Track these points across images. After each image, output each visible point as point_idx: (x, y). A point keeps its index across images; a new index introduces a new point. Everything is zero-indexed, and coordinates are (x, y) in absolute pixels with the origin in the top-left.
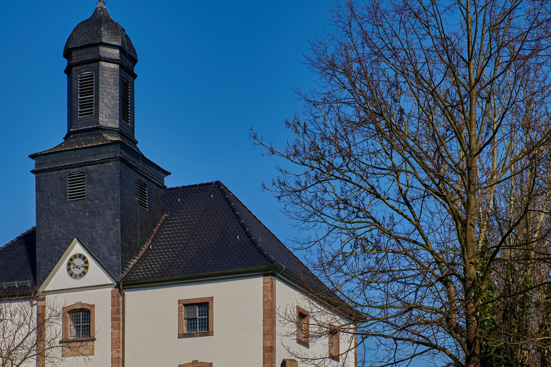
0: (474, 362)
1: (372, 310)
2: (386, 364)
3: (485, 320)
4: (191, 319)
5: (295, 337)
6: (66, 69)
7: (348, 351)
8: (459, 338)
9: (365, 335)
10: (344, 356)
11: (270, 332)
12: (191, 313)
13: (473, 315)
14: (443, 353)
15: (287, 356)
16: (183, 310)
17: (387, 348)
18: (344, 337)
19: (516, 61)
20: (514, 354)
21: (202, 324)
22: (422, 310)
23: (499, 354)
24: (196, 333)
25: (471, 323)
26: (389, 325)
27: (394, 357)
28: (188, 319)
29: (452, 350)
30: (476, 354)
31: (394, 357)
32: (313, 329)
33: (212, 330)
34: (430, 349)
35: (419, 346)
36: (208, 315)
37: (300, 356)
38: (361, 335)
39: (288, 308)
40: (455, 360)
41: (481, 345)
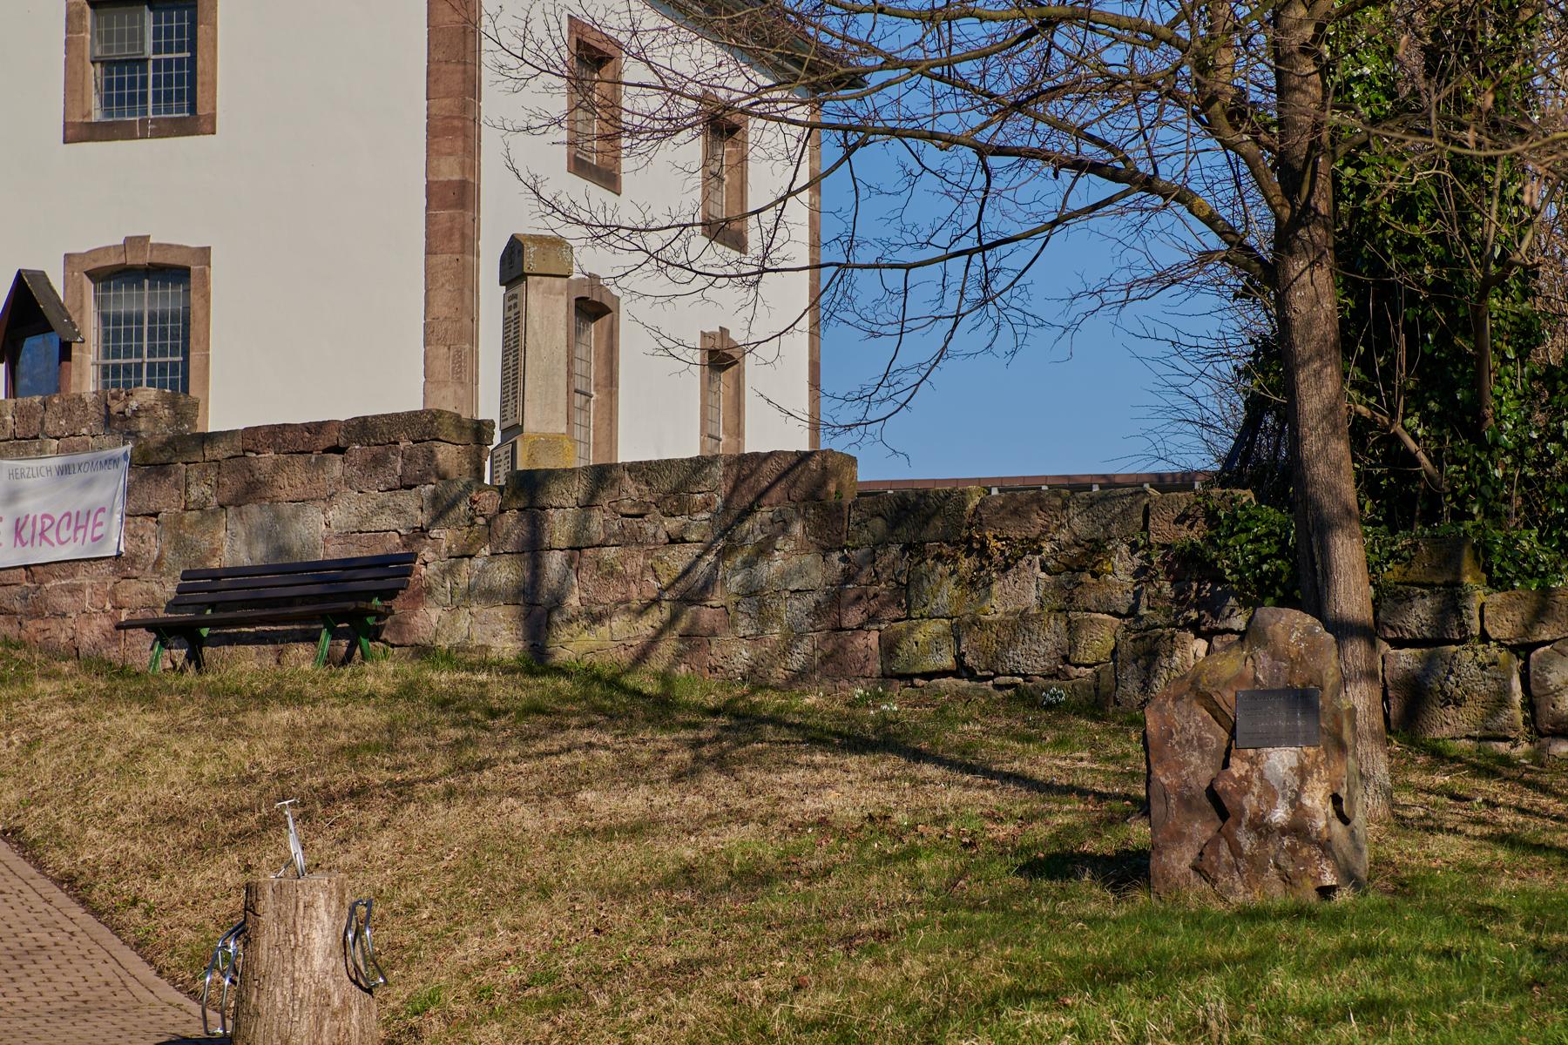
0: (1309, 247)
1: (889, 30)
2: (943, 252)
3: (1352, 79)
4: (120, 63)
5: (563, 136)
6: (188, 135)
7: (784, 199)
8: (1250, 148)
9: (856, 135)
10: (768, 217)
11: (456, 123)
12: (121, 38)
13: (1304, 51)
14: (1181, 209)
15: (531, 222)
16: (88, 21)
17: (949, 187)
18: (767, 136)
19: (1185, 120)
20: (1473, 222)
21: (168, 82)
22: (1093, 29)
23: (1411, 219)
24: (143, 123)
25: (1295, 89)
26: (958, 91)
27: (978, 225)
28: (108, 64)
29: (1219, 199)
30: (1317, 213)
31: (978, 225)
32: (639, 104)
33: (208, 111)
34: (1125, 194)
35: (1083, 181)
36: (193, 47)
37: (585, 217)
38: (840, 133)
39: (536, 13)
40: (1232, 238)
41: (1336, 179)
